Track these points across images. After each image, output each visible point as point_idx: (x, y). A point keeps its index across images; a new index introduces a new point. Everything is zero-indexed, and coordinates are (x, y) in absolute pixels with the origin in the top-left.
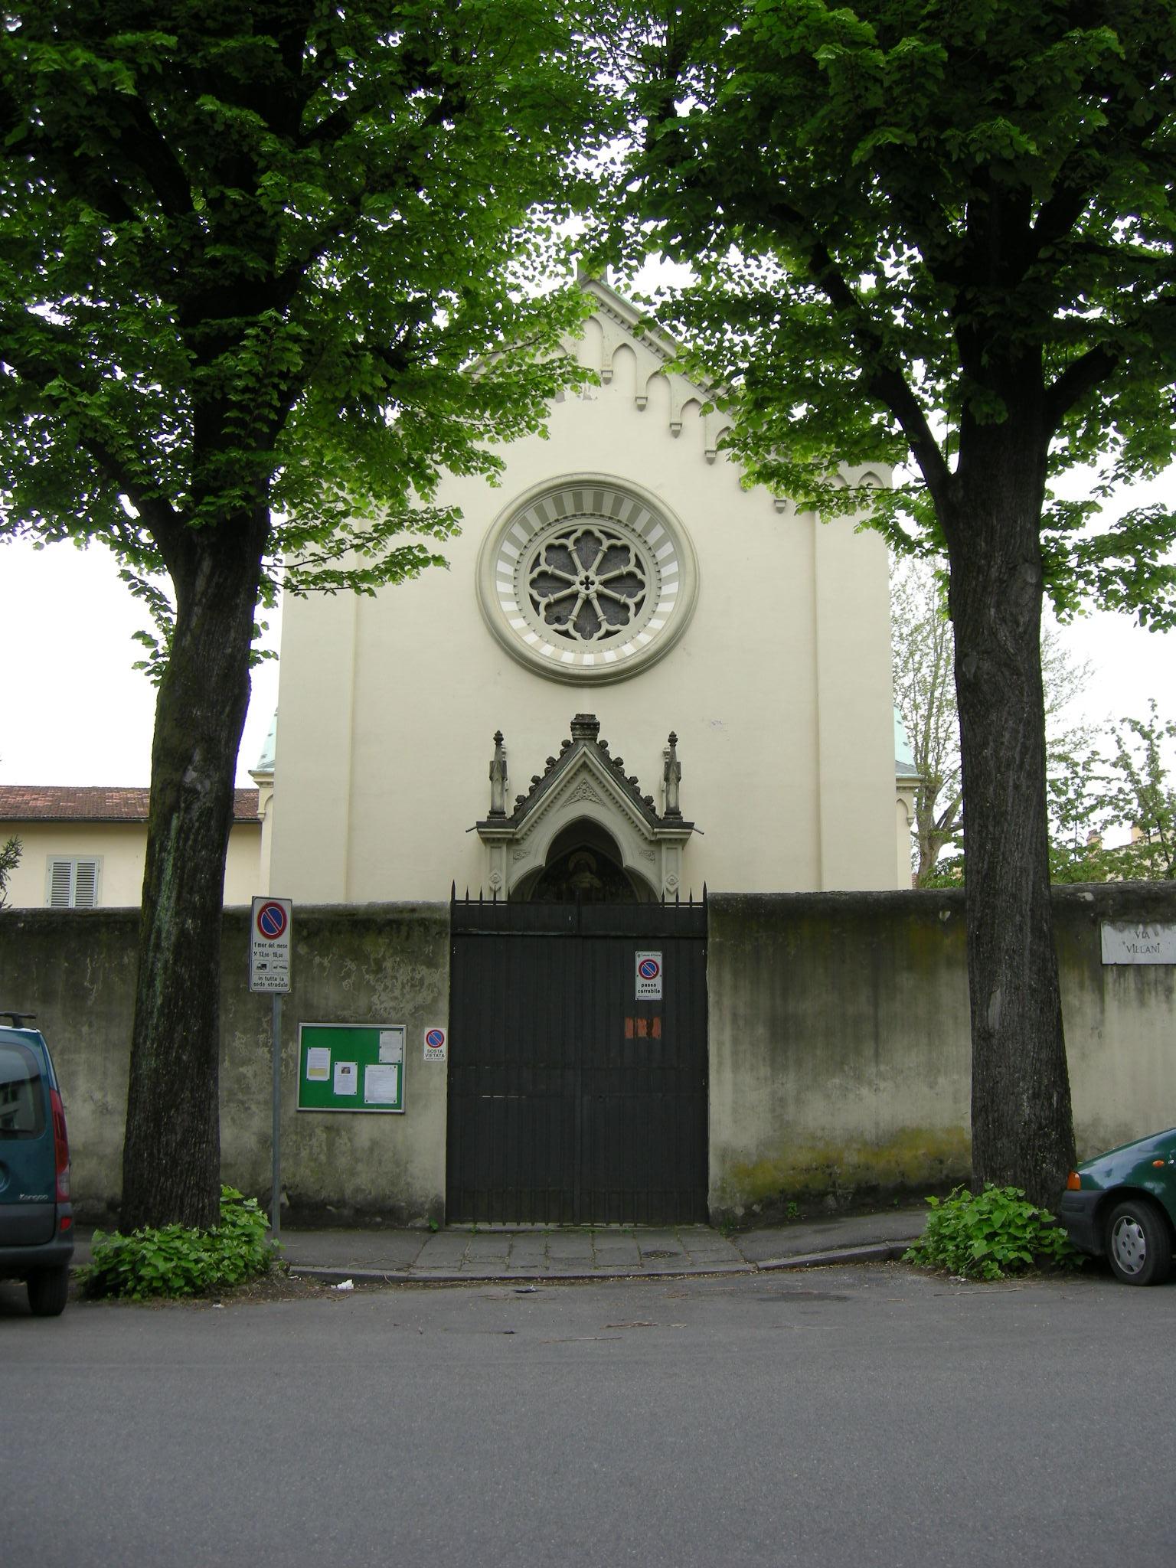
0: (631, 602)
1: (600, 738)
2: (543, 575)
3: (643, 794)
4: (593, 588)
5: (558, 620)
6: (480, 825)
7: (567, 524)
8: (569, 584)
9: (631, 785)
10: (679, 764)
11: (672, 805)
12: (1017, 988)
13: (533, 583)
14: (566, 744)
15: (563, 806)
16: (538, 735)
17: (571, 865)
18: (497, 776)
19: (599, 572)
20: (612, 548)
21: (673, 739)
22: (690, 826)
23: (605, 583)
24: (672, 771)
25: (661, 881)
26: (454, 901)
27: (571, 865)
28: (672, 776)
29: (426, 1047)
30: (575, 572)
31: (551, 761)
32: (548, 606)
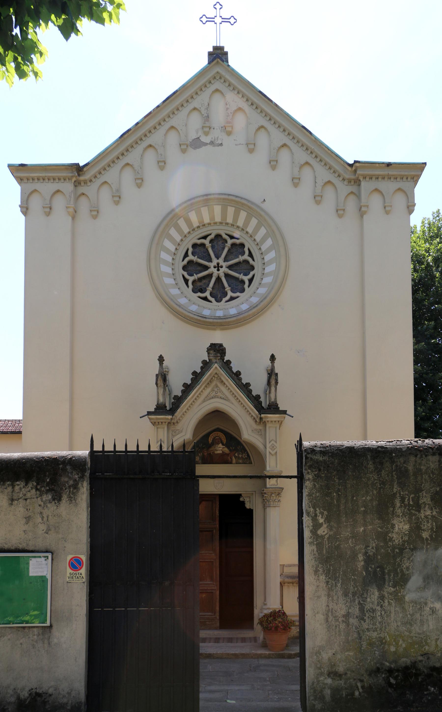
0: (246, 279)
1: (226, 358)
2: (190, 262)
3: (254, 393)
4: (215, 270)
5: (202, 291)
6: (149, 413)
7: (205, 229)
8: (207, 268)
9: (246, 388)
13: (184, 268)
14: (204, 362)
15: (204, 401)
16: (186, 351)
17: (210, 440)
18: (160, 382)
19: (225, 260)
20: (233, 245)
21: (273, 358)
22: (285, 412)
23: (230, 267)
24: (272, 375)
25: (265, 447)
26: (92, 453)
28: (273, 382)
29: (69, 571)
30: (210, 260)
31: (194, 373)
32: (194, 282)
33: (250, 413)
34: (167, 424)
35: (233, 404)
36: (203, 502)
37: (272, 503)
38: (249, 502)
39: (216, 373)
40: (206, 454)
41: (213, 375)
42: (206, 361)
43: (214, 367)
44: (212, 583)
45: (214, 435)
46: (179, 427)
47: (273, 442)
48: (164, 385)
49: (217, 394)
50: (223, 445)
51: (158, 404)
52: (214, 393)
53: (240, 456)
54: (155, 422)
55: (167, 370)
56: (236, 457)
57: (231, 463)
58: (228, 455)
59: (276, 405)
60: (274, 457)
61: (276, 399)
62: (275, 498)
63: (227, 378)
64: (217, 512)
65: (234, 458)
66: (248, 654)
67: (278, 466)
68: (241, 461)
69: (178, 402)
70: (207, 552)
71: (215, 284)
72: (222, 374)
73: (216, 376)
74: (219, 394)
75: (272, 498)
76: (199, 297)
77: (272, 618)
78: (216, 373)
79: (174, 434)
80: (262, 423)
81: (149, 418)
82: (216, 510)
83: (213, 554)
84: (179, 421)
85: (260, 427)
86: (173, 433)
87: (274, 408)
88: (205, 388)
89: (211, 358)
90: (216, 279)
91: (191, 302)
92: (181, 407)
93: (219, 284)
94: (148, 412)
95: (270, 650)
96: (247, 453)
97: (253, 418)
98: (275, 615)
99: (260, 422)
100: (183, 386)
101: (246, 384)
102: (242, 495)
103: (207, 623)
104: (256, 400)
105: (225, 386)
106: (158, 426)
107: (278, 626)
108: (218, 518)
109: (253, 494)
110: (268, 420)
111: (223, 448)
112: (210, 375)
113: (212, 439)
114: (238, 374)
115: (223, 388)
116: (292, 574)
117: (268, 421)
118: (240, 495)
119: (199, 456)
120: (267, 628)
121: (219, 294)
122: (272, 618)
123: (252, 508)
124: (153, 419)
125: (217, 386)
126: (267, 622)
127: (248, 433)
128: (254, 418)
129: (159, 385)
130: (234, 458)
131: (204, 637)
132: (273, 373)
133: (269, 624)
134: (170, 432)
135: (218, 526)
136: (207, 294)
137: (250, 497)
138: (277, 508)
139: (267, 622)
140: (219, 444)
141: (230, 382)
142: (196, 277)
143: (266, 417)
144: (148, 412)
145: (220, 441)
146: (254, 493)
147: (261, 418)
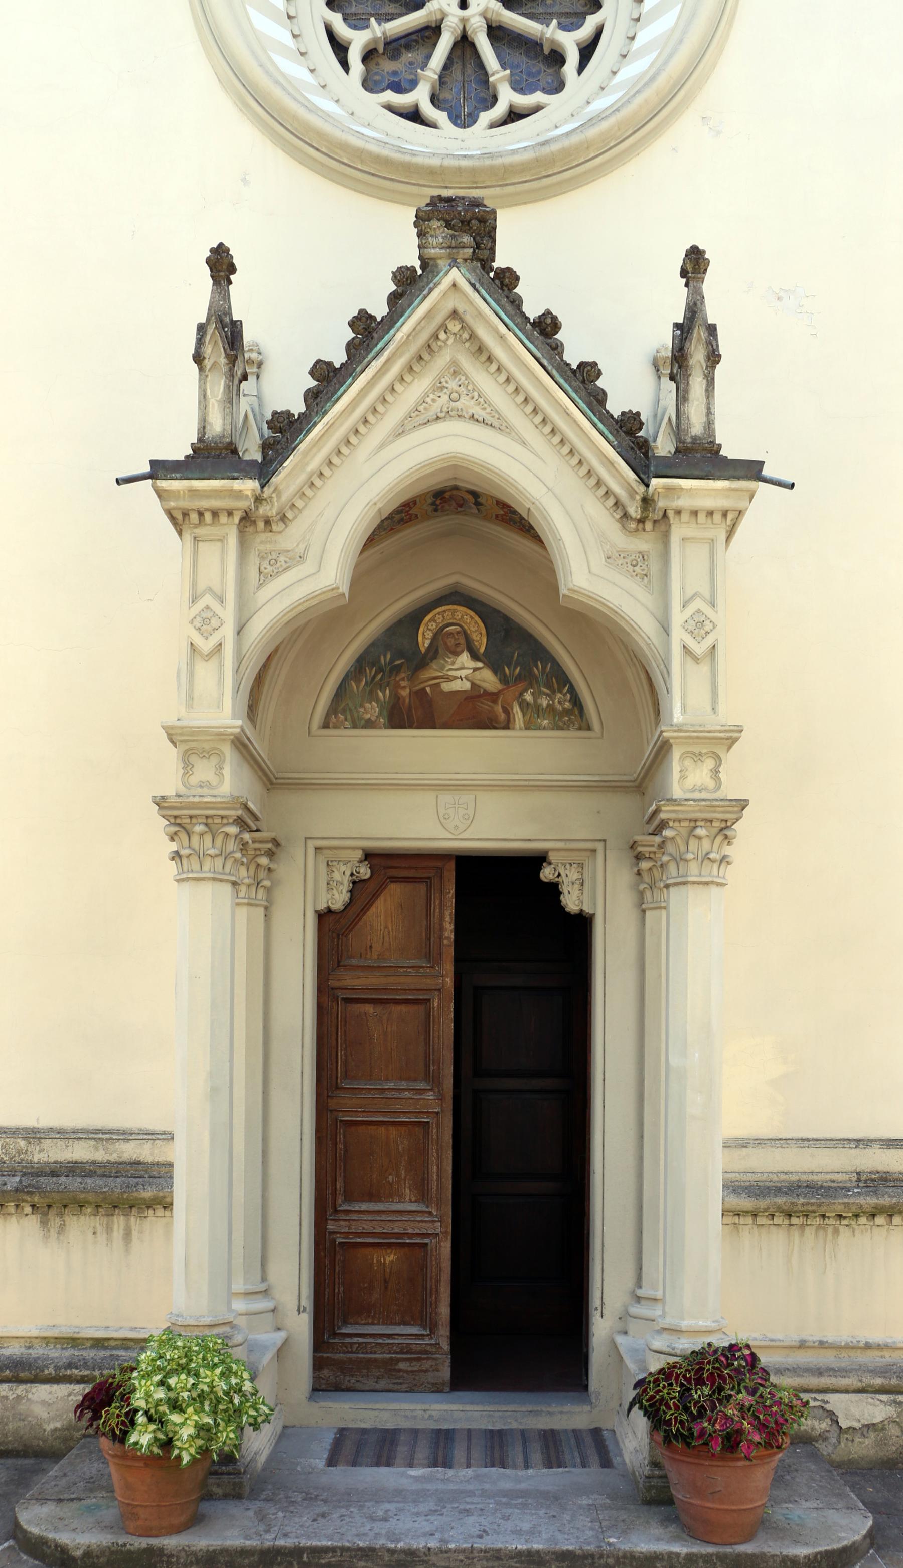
3: (615, 407)
6: (160, 470)
9: (584, 379)
10: (712, 330)
11: (696, 428)
12: (349, 1494)
15: (400, 432)
17: (424, 639)
18: (216, 353)
22: (752, 470)
24: (691, 348)
25: (666, 629)
27: (424, 639)
28: (697, 355)
33: (599, 483)
34: (237, 520)
35: (524, 443)
36: (393, 886)
37: (693, 867)
38: (576, 886)
39: (454, 314)
40: (405, 693)
41: (439, 319)
42: (413, 269)
43: (446, 282)
44: (423, 1208)
45: (439, 619)
46: (289, 538)
47: (697, 604)
48: (232, 361)
49: (458, 405)
50: (475, 656)
51: (200, 440)
52: (445, 398)
53: (544, 702)
54: (185, 514)
55: (254, 356)
56: (524, 706)
57: (507, 726)
58: (493, 697)
59: (714, 450)
60: (705, 668)
61: (709, 425)
62: (706, 844)
63: (503, 329)
64: (449, 927)
65: (516, 709)
66: (592, 1556)
67: (722, 707)
68: (545, 722)
69: (285, 431)
70: (404, 1085)
71: (447, 66)
72: (480, 314)
73: (455, 327)
74: (466, 404)
75: (693, 844)
76: (390, 108)
77: (707, 1391)
78: (454, 314)
79: (270, 569)
80: (649, 525)
81: (160, 493)
82: (442, 918)
83: (430, 1095)
84: (290, 515)
85: (644, 543)
86: (265, 564)
87: (701, 457)
88: (408, 378)
89: (432, 252)
90: (455, 45)
91: (357, 112)
92: (302, 447)
93: (464, 66)
94: (153, 463)
95: (693, 1533)
96: (572, 690)
97: (611, 501)
98: (721, 1377)
99: (641, 521)
100: (312, 373)
101: (582, 365)
102: (552, 857)
103: (402, 1366)
104: (627, 431)
105: (494, 367)
106: (200, 531)
107: (740, 1431)
108: (452, 951)
109: (594, 851)
110: (681, 503)
111: (475, 669)
112: (429, 315)
113: (429, 635)
114: (546, 328)
115: (484, 381)
116: (750, 1177)
117: (678, 512)
118: (539, 860)
119: (377, 700)
120: (686, 1439)
121: (464, 90)
122: (707, 1391)
123: (587, 909)
124: (175, 494)
125: (456, 371)
126: (687, 1409)
127: (588, 556)
128: (617, 504)
129: (208, 363)
130: (516, 709)
131: (390, 1426)
132: (699, 321)
133: (694, 1418)
134: (253, 561)
135: (449, 981)
136: (420, 96)
137: (581, 865)
138: (714, 889)
139: (687, 1409)
140: (457, 654)
141: (515, 351)
142: (377, 30)
143: (669, 489)
144: (153, 463)
145: (462, 640)
146: (599, 846)
147: (647, 501)
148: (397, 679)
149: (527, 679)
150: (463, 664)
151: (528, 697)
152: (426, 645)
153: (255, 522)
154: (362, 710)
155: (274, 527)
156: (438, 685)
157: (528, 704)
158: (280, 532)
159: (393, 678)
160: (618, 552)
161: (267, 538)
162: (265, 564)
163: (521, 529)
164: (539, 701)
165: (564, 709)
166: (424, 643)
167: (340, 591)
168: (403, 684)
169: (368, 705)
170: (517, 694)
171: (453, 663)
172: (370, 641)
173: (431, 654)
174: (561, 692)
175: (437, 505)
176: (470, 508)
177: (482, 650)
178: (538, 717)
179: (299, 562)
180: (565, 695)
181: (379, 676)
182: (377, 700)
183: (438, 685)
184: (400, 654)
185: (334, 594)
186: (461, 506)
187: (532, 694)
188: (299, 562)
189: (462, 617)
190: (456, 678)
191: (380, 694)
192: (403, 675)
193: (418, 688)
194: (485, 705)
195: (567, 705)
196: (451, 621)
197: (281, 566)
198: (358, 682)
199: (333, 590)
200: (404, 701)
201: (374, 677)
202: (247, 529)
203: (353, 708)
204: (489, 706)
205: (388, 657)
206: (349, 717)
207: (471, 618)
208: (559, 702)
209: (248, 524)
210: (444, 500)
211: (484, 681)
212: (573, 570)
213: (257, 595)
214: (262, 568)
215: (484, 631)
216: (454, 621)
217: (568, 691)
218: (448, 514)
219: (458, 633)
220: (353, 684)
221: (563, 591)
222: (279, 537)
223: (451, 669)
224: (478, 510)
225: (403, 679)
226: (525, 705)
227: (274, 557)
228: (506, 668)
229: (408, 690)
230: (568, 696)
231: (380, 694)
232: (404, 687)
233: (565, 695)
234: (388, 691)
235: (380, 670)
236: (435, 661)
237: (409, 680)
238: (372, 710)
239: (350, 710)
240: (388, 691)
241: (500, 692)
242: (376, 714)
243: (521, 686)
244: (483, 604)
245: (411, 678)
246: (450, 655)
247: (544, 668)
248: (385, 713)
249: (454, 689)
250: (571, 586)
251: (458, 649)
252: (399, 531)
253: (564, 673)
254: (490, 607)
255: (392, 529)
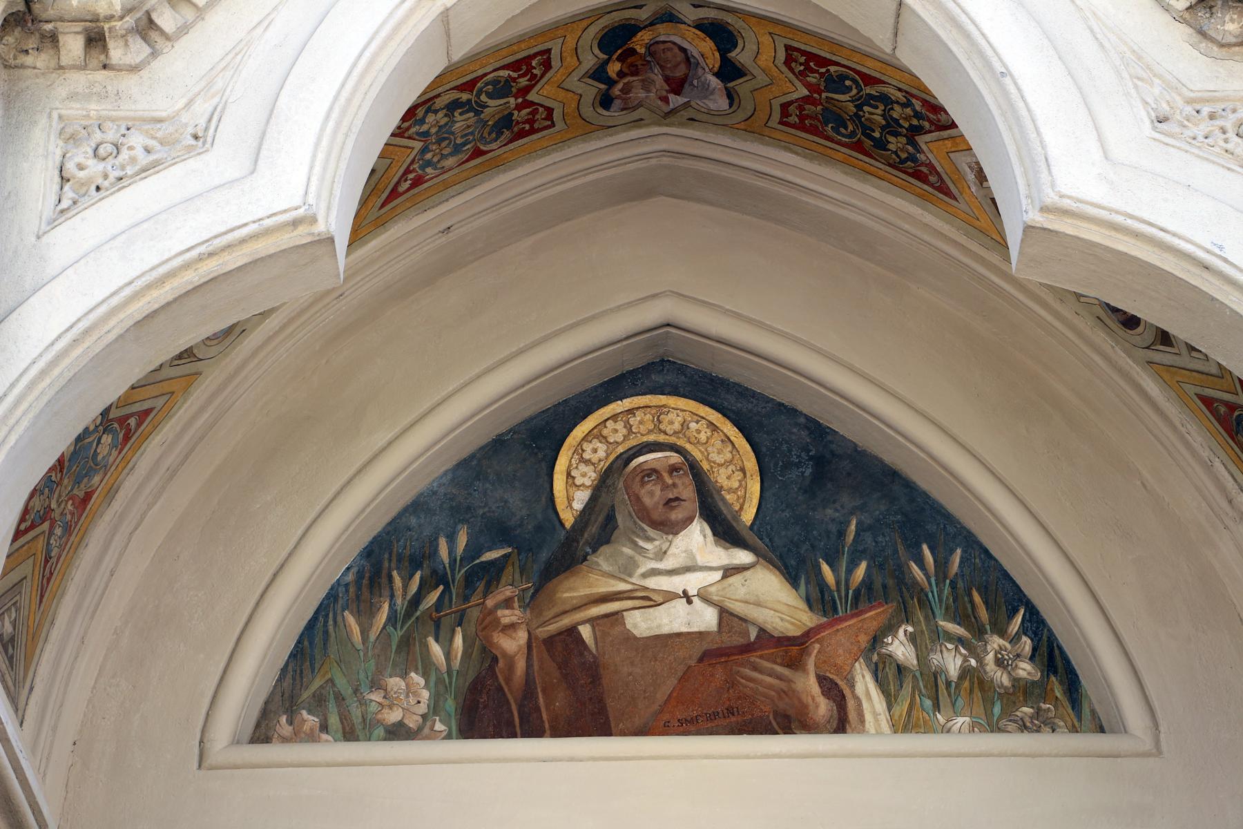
40: (512, 644)
45: (616, 432)
50: (726, 532)
53: (951, 662)
56: (890, 676)
58: (791, 649)
65: (865, 685)
86: (82, 154)
96: (1036, 624)
111: (730, 571)
113: (587, 477)
119: (427, 667)
130: (865, 685)
140: (671, 528)
145: (687, 490)
148: (490, 603)
149: (894, 594)
150: (691, 555)
151: (900, 648)
152: (578, 506)
153: (53, 39)
154: (376, 697)
155: (116, 53)
156: (616, 617)
157: (901, 669)
158: (134, 69)
159: (475, 600)
160: (1189, 102)
161: (92, 85)
162: (82, 154)
163: (858, 147)
164: (935, 659)
165: (1016, 681)
166: (570, 500)
167: (321, 227)
168: (506, 616)
169: (395, 683)
170: (864, 640)
171: (661, 555)
172: (407, 498)
173: (593, 529)
174: (1002, 633)
175: (611, 83)
176: (706, 91)
177: (748, 516)
178: (937, 706)
179: (190, 148)
180: (1015, 640)
181: (433, 597)
182: (427, 667)
183: (616, 617)
184: (500, 532)
185: (300, 236)
186: (677, 86)
187: (912, 638)
188: (190, 148)
189: (685, 425)
190: (670, 596)
191: (436, 649)
192: (507, 592)
193: (553, 628)
194: (764, 676)
195: (1026, 669)
196: (652, 438)
197: (133, 160)
198: (366, 613)
199: (295, 223)
200: (511, 666)
201: (416, 601)
202: (28, 60)
203: (347, 691)
204: (779, 677)
205: (462, 540)
206: (334, 720)
207: (713, 427)
208: (999, 662)
209: (32, 43)
210: (634, 65)
211: (758, 604)
212: (1053, 152)
213: (44, 239)
214: (70, 166)
215: (751, 463)
216: (661, 438)
217: (1024, 630)
218: (638, 123)
219: (673, 469)
220: (351, 620)
221: (1020, 211)
222: (129, 83)
223: (654, 572)
224: (731, 96)
225: (507, 604)
226: (891, 672)
227: (111, 135)
228: (825, 568)
229: (522, 636)
230: (1027, 644)
231: (436, 649)
232: (512, 626)
233: (1015, 640)
234: (459, 641)
235: (437, 578)
236: (605, 549)
237: (524, 606)
238: (410, 694)
239: (339, 698)
240: (459, 641)
241: (808, 634)
242: (423, 708)
243: (873, 617)
244: (744, 393)
245: (534, 600)
246: (651, 532)
247: (942, 565)
248: (450, 705)
249: (666, 630)
250: (1051, 198)
251: (676, 515)
252: (498, 165)
253: (1006, 575)
254: (769, 400)
255: (478, 153)
